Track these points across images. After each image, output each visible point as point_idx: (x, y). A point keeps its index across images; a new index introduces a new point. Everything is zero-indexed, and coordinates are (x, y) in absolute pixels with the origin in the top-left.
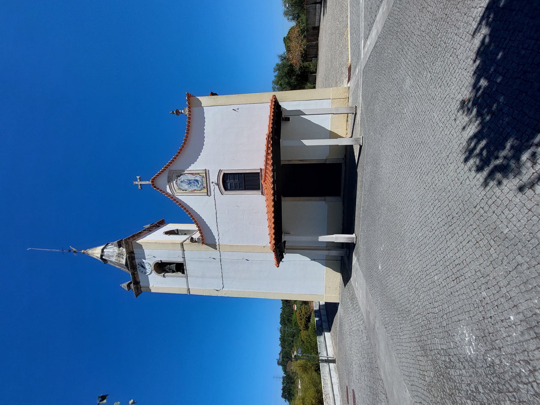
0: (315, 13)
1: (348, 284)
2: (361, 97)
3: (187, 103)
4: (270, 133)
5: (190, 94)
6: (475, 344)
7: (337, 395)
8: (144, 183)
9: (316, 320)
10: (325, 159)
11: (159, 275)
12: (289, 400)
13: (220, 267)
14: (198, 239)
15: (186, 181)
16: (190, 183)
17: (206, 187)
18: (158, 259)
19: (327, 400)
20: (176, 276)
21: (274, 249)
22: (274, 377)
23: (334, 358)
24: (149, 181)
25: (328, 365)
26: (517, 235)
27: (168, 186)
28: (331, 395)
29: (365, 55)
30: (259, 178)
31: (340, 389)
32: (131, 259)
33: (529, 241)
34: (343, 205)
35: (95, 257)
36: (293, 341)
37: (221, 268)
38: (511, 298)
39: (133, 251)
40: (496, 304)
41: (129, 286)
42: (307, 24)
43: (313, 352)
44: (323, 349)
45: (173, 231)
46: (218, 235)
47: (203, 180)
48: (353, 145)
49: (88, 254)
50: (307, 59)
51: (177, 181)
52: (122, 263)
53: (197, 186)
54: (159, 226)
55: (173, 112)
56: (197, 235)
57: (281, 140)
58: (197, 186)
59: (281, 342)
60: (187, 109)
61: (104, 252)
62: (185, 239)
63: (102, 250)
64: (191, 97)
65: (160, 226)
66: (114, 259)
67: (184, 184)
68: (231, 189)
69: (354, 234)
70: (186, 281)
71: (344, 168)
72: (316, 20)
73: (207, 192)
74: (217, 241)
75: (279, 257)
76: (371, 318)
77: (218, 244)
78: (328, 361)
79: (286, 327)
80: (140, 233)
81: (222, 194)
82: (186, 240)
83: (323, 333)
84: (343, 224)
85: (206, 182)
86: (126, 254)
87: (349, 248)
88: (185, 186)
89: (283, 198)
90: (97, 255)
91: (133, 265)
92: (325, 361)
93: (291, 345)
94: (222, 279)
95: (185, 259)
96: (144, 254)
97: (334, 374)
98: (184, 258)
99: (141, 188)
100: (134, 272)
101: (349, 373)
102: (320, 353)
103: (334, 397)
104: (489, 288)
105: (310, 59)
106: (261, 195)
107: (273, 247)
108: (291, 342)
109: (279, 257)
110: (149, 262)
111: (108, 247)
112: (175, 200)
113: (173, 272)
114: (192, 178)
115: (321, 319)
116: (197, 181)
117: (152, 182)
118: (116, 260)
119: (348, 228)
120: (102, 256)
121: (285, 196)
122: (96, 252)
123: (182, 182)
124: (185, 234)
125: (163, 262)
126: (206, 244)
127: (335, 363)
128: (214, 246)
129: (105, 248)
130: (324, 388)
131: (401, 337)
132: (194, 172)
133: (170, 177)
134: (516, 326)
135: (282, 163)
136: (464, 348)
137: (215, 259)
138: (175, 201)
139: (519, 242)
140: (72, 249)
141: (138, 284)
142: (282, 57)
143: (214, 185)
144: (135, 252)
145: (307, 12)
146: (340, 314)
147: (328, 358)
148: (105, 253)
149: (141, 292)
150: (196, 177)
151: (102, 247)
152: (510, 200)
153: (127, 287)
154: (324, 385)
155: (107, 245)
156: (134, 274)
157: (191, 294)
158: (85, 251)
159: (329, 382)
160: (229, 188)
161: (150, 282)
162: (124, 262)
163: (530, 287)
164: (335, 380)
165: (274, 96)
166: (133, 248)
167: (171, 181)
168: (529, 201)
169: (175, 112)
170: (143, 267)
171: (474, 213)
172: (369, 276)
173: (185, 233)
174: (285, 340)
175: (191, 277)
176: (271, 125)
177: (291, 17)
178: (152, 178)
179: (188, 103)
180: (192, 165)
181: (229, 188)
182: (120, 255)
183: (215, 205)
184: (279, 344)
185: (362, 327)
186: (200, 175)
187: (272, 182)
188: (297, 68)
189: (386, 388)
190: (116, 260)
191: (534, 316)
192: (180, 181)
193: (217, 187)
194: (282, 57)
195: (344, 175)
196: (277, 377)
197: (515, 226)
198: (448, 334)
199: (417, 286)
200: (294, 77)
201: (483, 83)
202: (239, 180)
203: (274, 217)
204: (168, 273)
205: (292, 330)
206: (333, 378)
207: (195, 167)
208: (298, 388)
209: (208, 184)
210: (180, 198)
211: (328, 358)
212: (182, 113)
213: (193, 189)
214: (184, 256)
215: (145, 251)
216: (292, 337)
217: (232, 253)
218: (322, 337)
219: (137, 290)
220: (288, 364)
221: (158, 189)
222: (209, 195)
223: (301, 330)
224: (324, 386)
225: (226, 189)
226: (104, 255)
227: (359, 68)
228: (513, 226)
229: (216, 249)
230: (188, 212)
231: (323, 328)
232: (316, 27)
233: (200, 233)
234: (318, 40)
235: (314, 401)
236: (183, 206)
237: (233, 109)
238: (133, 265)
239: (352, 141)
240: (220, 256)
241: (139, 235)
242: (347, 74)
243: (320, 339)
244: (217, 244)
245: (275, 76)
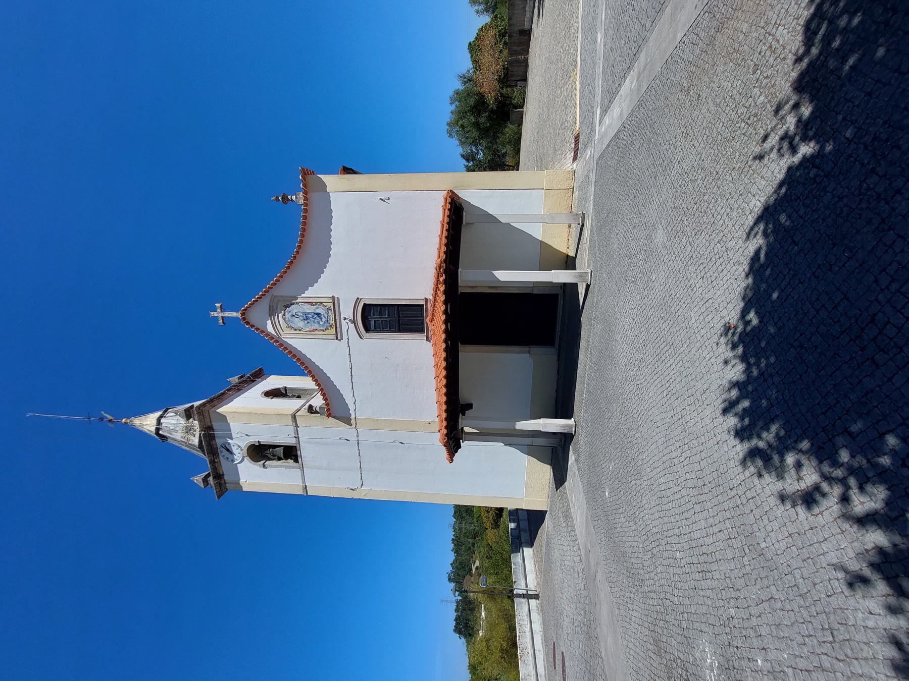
0: (524, 8)
1: (561, 488)
2: (591, 202)
3: (301, 185)
4: (441, 263)
5: (307, 170)
6: (717, 673)
7: (539, 651)
8: (229, 316)
9: (511, 529)
10: (531, 287)
11: (257, 465)
12: (466, 636)
13: (358, 453)
14: (320, 408)
15: (300, 314)
16: (307, 318)
17: (334, 324)
18: (254, 439)
19: (524, 658)
20: (284, 466)
21: (446, 442)
23: (536, 591)
24: (237, 312)
25: (527, 603)
26: (774, 558)
27: (269, 322)
28: (530, 650)
29: (602, 138)
30: (422, 309)
31: (543, 641)
32: (208, 437)
33: (786, 575)
34: (558, 360)
35: (146, 430)
36: (473, 545)
37: (358, 455)
38: (760, 635)
39: (212, 425)
40: (745, 634)
41: (205, 480)
42: (510, 25)
43: (506, 568)
44: (521, 576)
45: (278, 389)
46: (355, 403)
47: (330, 314)
48: (577, 283)
49: (134, 425)
50: (508, 83)
51: (284, 315)
52: (193, 443)
53: (319, 323)
54: (254, 381)
55: (277, 198)
56: (318, 401)
57: (460, 270)
58: (319, 323)
60: (301, 195)
61: (162, 424)
62: (298, 407)
63: (157, 419)
64: (308, 174)
65: (256, 380)
66: (178, 436)
67: (296, 320)
68: (377, 330)
69: (572, 419)
70: (302, 474)
71: (562, 302)
72: (526, 19)
73: (337, 333)
74: (352, 412)
75: (453, 443)
76: (592, 562)
77: (354, 417)
78: (527, 596)
79: (464, 522)
80: (222, 394)
81: (361, 338)
82: (300, 409)
83: (521, 549)
84: (556, 391)
85: (333, 316)
86: (198, 430)
87: (566, 439)
88: (298, 322)
89: (461, 347)
90: (149, 428)
91: (211, 448)
92: (522, 596)
93: (471, 551)
94: (360, 473)
95: (299, 439)
96: (230, 430)
97: (535, 616)
98: (297, 438)
99: (223, 323)
100: (214, 459)
101: (558, 626)
102: (515, 582)
103: (535, 654)
104: (738, 608)
105: (514, 83)
106: (425, 342)
107: (444, 439)
109: (453, 443)
110: (239, 443)
111: (167, 416)
112: (281, 345)
113: (280, 459)
115: (518, 526)
116: (319, 315)
117: (243, 314)
118: (182, 437)
119: (563, 409)
120: (158, 430)
121: (466, 342)
122: (148, 423)
123: (294, 316)
124: (299, 397)
125: (262, 443)
126: (334, 417)
127: (538, 599)
128: (347, 420)
129: (162, 417)
130: (519, 640)
131: (630, 612)
132: (313, 299)
133: (273, 306)
134: (762, 674)
135: (461, 290)
136: (704, 671)
137: (349, 441)
138: (282, 348)
139: (776, 569)
140: (105, 416)
141: (221, 478)
142: (465, 78)
143: (347, 323)
144: (214, 428)
145: (511, 5)
146: (548, 528)
147: (527, 591)
149: (225, 490)
150: (317, 308)
151: (158, 414)
152: (771, 507)
153: (203, 482)
154: (520, 634)
155: (166, 411)
156: (214, 461)
157: (309, 494)
158: (128, 421)
159: (528, 630)
160: (373, 328)
161: (240, 475)
162: (196, 441)
163: (781, 635)
164: (537, 627)
165: (449, 192)
166: (212, 421)
167: (274, 314)
168: (791, 523)
169: (280, 198)
170: (228, 450)
171: (730, 497)
172: (593, 491)
173: (297, 394)
174: (461, 542)
175: (308, 468)
176: (444, 249)
177: (481, 7)
178: (242, 308)
179: (303, 185)
180: (310, 288)
181: (373, 328)
182: (188, 430)
183: (350, 355)
185: (578, 568)
186: (324, 306)
187: (443, 291)
188: (491, 99)
189: (608, 673)
190: (182, 437)
191: (782, 673)
192: (290, 314)
193: (352, 326)
194: (465, 78)
195: (561, 313)
196: (447, 601)
197: (773, 545)
198: (688, 643)
199: (655, 551)
200: (486, 114)
201: (752, 316)
202: (389, 315)
203: (446, 386)
204: (271, 461)
205: (472, 527)
206: (534, 623)
208: (479, 634)
209: (338, 321)
210: (290, 341)
211: (527, 592)
212: (292, 200)
213: (312, 328)
214: (298, 435)
215: (231, 425)
216: (471, 538)
217: (377, 432)
218: (520, 554)
219: (219, 487)
220: (465, 580)
221: (253, 326)
222: (339, 338)
223: (487, 529)
224: (519, 636)
225: (367, 329)
226: (161, 429)
227: (591, 152)
228: (771, 544)
229: (351, 425)
230: (304, 364)
231: (522, 541)
232: (524, 30)
233: (322, 395)
234: (527, 52)
235: (505, 644)
236: (295, 356)
237: (381, 199)
238: (211, 448)
239: (575, 277)
240: (358, 436)
241: (221, 398)
242: (573, 145)
243: (516, 559)
244: (353, 416)
245: (452, 112)
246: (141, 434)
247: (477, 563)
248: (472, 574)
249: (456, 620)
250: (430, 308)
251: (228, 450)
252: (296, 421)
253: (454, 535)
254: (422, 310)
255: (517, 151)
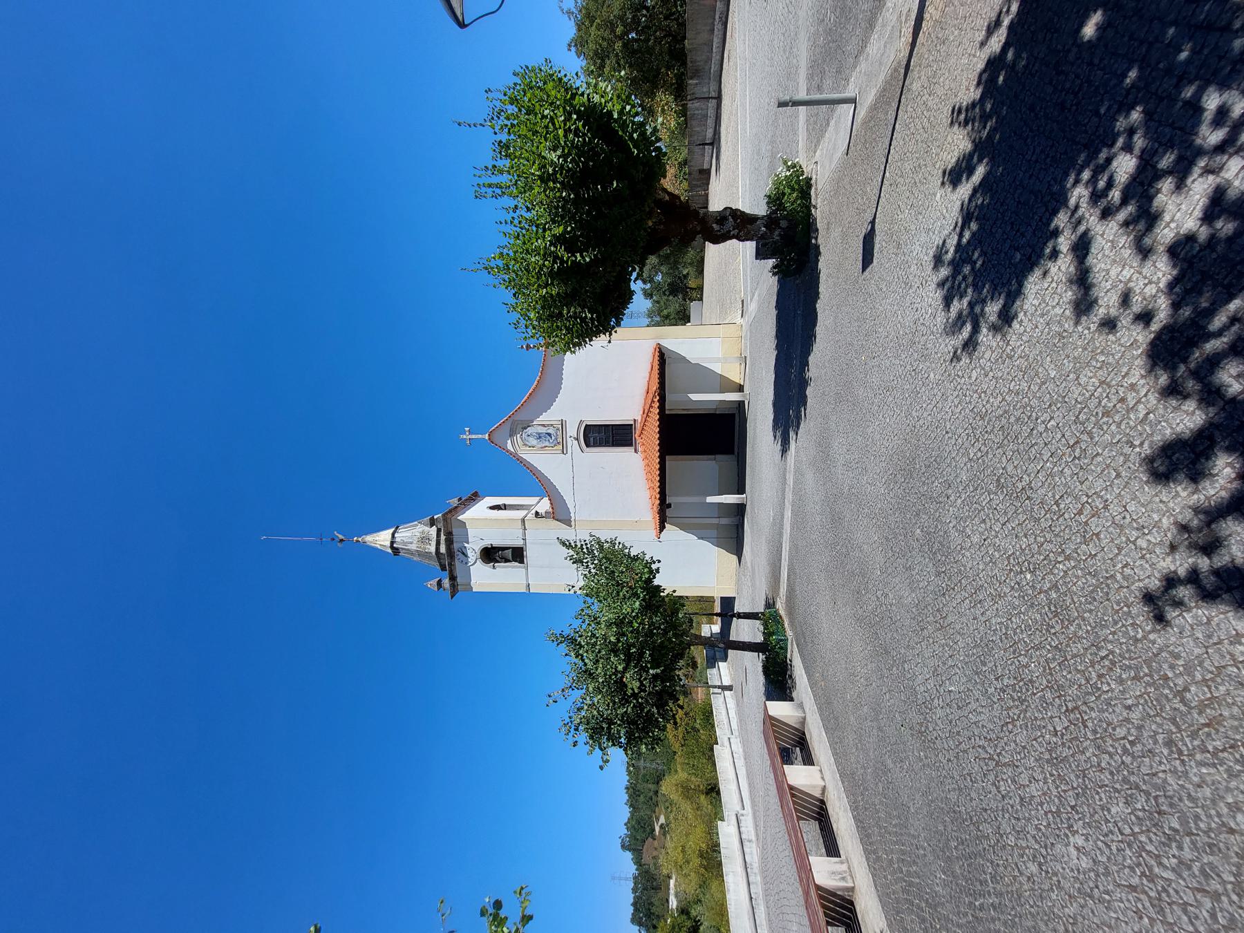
16: (540, 437)
18: (487, 543)
22: (613, 878)
27: (509, 442)
59: (630, 796)
68: (595, 445)
74: (572, 515)
78: (724, 688)
87: (740, 510)
88: (533, 441)
89: (667, 457)
108: (651, 794)
110: (473, 548)
114: (543, 430)
116: (549, 435)
119: (741, 489)
120: (392, 543)
135: (667, 412)
148: (398, 540)
170: (463, 553)
184: (626, 801)
207: (548, 417)
210: (524, 456)
218: (714, 671)
220: (645, 847)
246: (375, 552)
247: (662, 820)
248: (655, 835)
249: (634, 904)
250: (638, 426)
251: (463, 553)
252: (524, 525)
253: (628, 781)
254: (631, 428)
255: (701, 272)
